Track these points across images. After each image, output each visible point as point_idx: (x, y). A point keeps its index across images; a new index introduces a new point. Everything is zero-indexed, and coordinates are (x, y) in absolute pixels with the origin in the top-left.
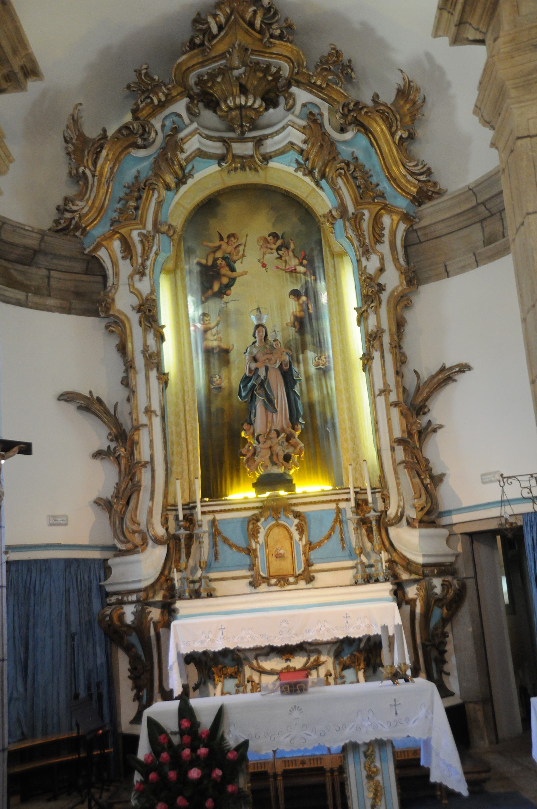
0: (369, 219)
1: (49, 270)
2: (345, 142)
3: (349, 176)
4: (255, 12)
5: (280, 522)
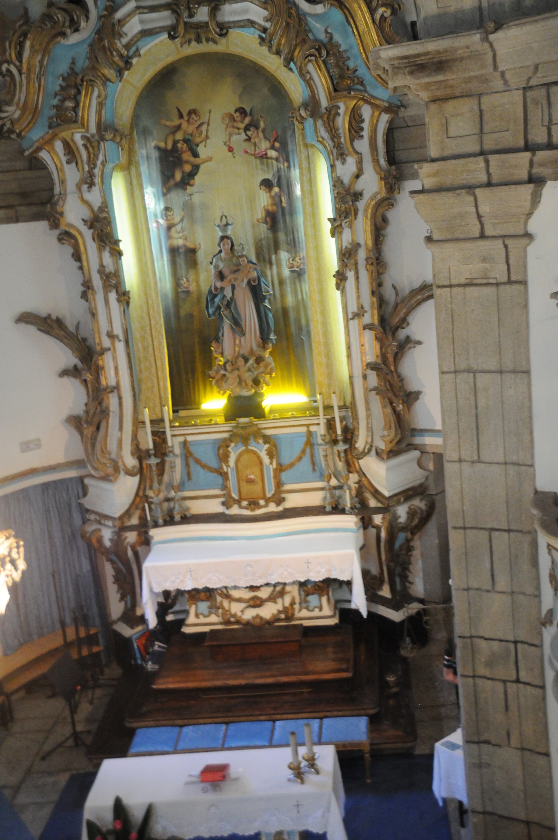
2: (316, 16)
3: (320, 62)
5: (250, 448)
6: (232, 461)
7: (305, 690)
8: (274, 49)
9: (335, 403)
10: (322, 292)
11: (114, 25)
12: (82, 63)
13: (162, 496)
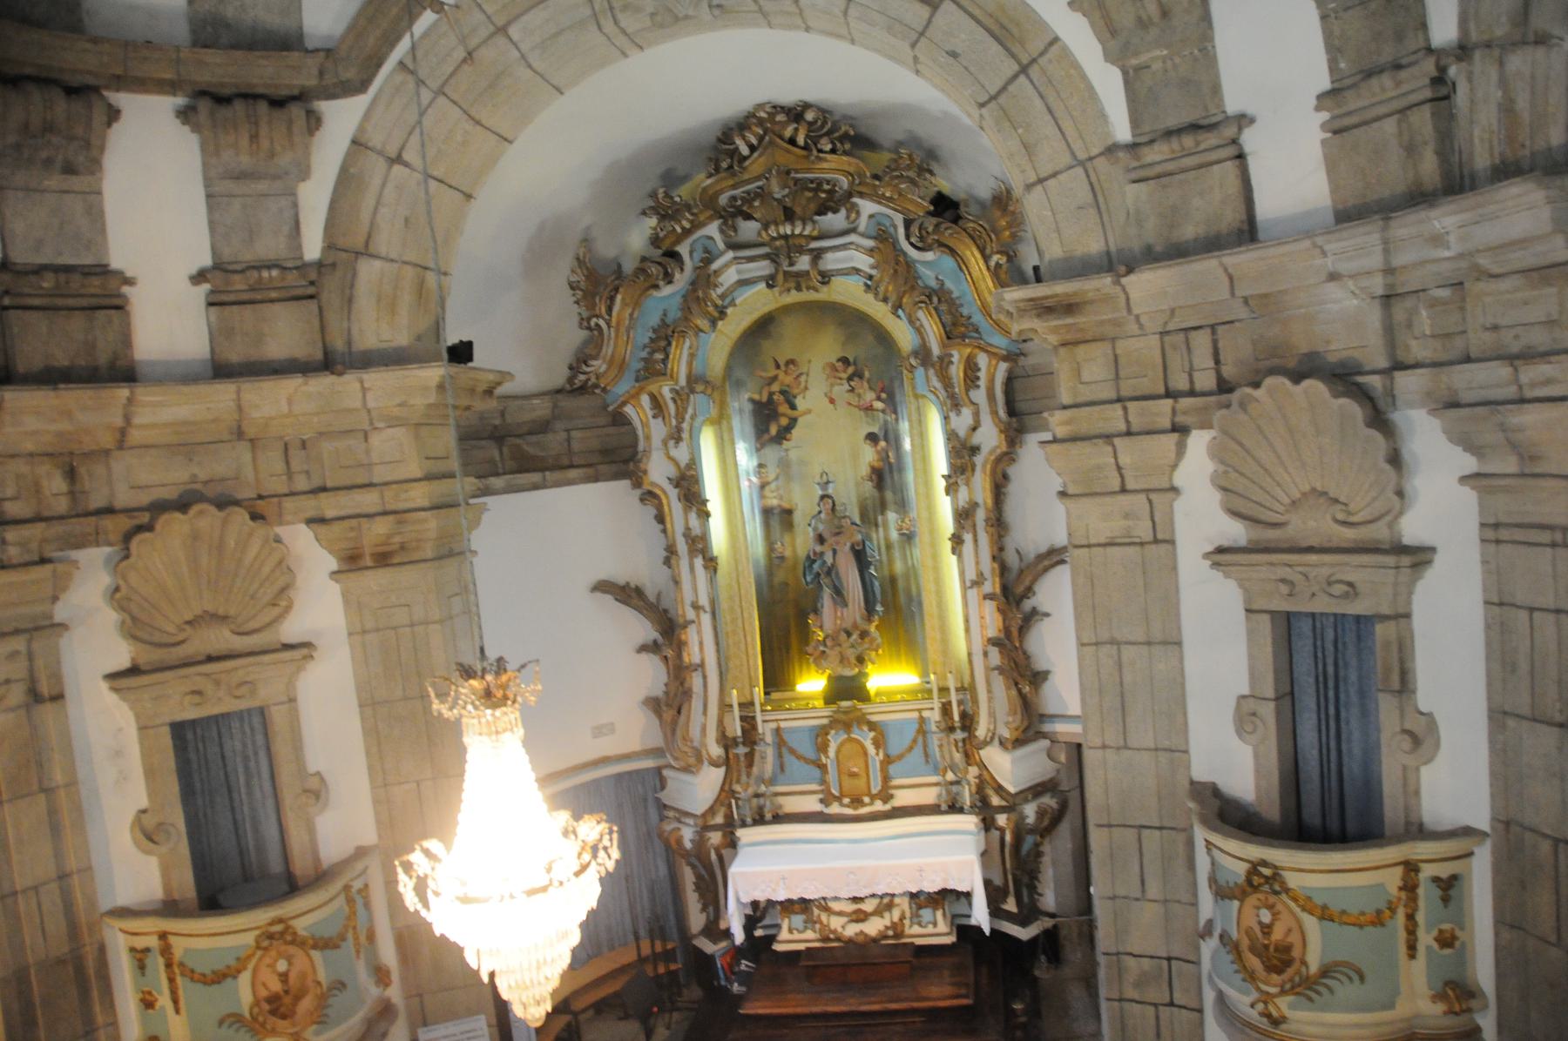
0: (959, 362)
1: (568, 431)
2: (926, 263)
4: (796, 130)
6: (832, 752)
7: (917, 1019)
8: (881, 296)
9: (951, 684)
10: (935, 557)
11: (709, 276)
12: (674, 314)
13: (751, 791)
